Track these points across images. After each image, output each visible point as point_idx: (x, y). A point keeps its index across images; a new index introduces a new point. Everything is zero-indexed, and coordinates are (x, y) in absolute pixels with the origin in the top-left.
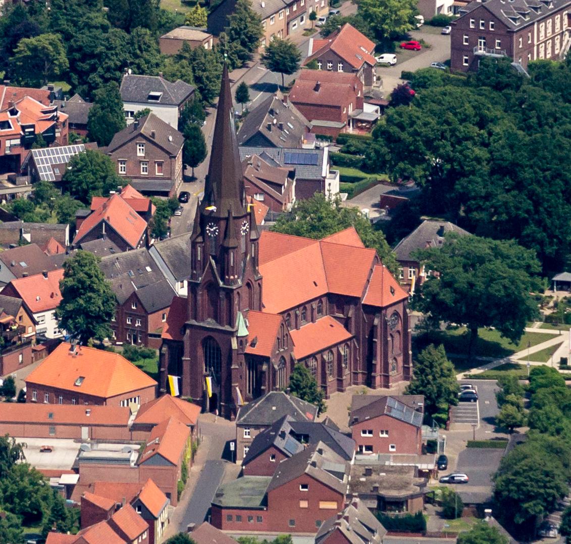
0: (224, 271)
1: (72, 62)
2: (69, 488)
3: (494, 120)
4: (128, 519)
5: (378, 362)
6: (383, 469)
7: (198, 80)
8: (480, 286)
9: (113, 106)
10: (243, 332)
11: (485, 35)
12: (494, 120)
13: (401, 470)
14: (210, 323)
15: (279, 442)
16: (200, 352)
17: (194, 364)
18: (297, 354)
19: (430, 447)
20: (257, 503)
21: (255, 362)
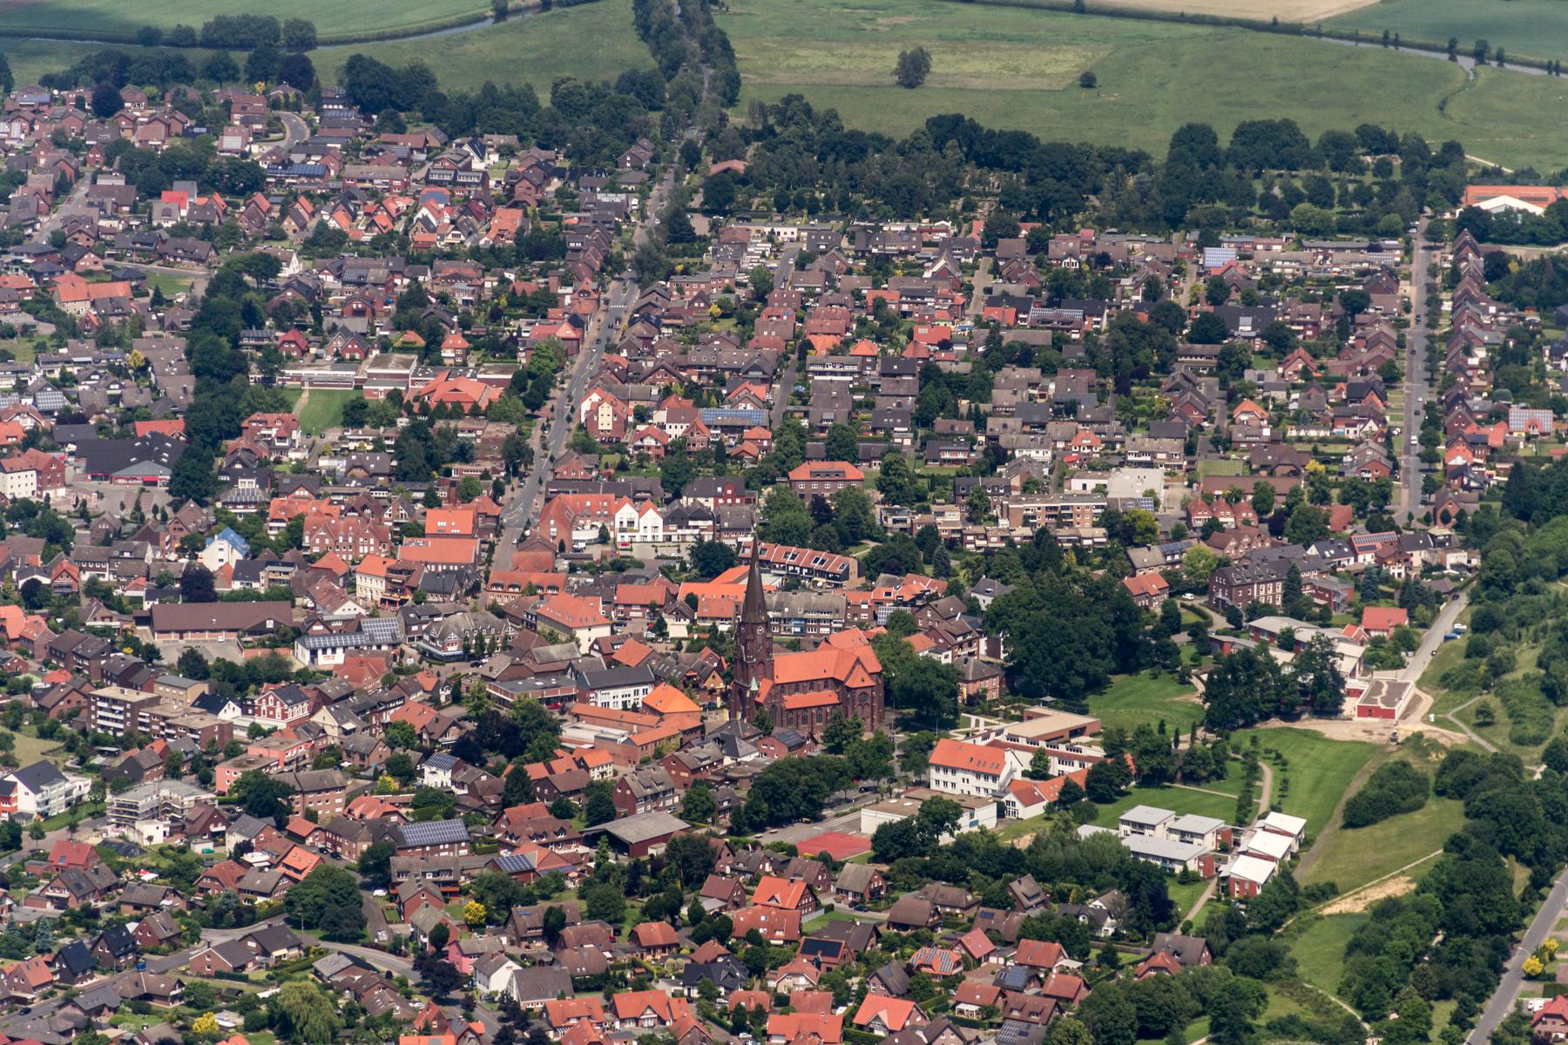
11: (1221, 586)
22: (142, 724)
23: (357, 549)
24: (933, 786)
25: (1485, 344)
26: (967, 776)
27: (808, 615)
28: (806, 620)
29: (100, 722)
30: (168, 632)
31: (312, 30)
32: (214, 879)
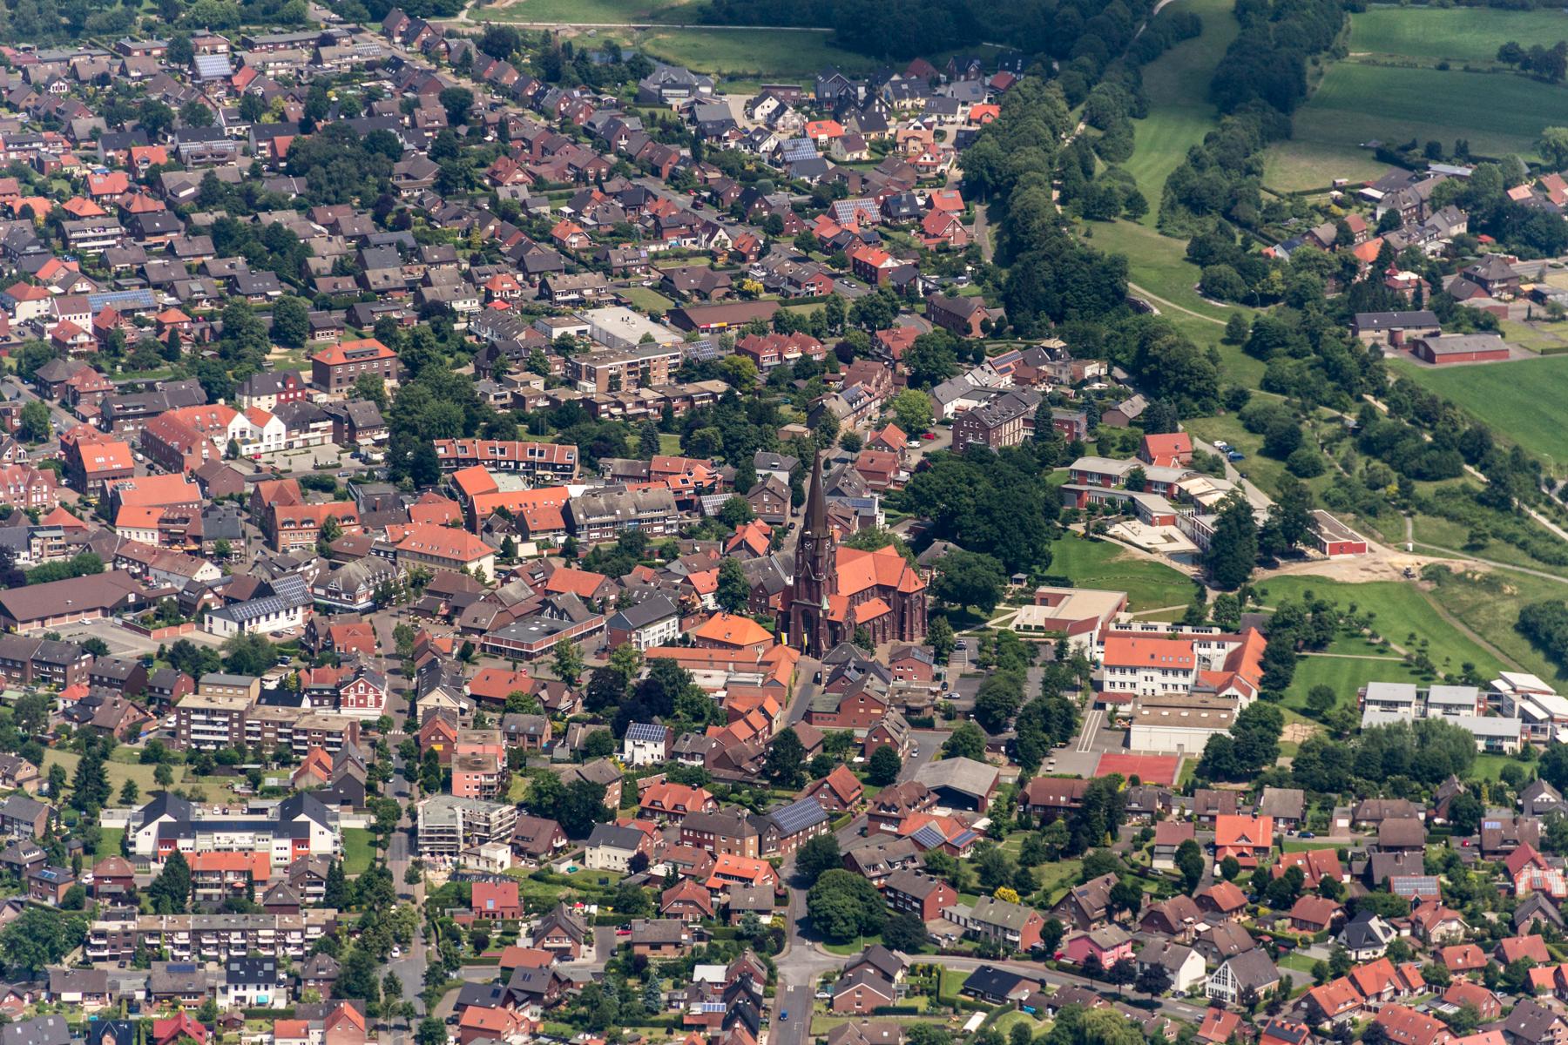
0: (815, 570)
1: (726, 444)
2: (721, 699)
5: (907, 626)
7: (801, 455)
8: (969, 581)
9: (749, 470)
10: (826, 607)
11: (973, 430)
13: (920, 691)
14: (806, 601)
18: (859, 621)
19: (938, 677)
20: (833, 709)
21: (833, 625)
22: (249, 733)
23: (28, 499)
24: (1107, 688)
26: (1149, 674)
27: (642, 515)
28: (640, 521)
29: (194, 736)
30: (30, 621)
31: (1517, 47)
32: (685, 902)
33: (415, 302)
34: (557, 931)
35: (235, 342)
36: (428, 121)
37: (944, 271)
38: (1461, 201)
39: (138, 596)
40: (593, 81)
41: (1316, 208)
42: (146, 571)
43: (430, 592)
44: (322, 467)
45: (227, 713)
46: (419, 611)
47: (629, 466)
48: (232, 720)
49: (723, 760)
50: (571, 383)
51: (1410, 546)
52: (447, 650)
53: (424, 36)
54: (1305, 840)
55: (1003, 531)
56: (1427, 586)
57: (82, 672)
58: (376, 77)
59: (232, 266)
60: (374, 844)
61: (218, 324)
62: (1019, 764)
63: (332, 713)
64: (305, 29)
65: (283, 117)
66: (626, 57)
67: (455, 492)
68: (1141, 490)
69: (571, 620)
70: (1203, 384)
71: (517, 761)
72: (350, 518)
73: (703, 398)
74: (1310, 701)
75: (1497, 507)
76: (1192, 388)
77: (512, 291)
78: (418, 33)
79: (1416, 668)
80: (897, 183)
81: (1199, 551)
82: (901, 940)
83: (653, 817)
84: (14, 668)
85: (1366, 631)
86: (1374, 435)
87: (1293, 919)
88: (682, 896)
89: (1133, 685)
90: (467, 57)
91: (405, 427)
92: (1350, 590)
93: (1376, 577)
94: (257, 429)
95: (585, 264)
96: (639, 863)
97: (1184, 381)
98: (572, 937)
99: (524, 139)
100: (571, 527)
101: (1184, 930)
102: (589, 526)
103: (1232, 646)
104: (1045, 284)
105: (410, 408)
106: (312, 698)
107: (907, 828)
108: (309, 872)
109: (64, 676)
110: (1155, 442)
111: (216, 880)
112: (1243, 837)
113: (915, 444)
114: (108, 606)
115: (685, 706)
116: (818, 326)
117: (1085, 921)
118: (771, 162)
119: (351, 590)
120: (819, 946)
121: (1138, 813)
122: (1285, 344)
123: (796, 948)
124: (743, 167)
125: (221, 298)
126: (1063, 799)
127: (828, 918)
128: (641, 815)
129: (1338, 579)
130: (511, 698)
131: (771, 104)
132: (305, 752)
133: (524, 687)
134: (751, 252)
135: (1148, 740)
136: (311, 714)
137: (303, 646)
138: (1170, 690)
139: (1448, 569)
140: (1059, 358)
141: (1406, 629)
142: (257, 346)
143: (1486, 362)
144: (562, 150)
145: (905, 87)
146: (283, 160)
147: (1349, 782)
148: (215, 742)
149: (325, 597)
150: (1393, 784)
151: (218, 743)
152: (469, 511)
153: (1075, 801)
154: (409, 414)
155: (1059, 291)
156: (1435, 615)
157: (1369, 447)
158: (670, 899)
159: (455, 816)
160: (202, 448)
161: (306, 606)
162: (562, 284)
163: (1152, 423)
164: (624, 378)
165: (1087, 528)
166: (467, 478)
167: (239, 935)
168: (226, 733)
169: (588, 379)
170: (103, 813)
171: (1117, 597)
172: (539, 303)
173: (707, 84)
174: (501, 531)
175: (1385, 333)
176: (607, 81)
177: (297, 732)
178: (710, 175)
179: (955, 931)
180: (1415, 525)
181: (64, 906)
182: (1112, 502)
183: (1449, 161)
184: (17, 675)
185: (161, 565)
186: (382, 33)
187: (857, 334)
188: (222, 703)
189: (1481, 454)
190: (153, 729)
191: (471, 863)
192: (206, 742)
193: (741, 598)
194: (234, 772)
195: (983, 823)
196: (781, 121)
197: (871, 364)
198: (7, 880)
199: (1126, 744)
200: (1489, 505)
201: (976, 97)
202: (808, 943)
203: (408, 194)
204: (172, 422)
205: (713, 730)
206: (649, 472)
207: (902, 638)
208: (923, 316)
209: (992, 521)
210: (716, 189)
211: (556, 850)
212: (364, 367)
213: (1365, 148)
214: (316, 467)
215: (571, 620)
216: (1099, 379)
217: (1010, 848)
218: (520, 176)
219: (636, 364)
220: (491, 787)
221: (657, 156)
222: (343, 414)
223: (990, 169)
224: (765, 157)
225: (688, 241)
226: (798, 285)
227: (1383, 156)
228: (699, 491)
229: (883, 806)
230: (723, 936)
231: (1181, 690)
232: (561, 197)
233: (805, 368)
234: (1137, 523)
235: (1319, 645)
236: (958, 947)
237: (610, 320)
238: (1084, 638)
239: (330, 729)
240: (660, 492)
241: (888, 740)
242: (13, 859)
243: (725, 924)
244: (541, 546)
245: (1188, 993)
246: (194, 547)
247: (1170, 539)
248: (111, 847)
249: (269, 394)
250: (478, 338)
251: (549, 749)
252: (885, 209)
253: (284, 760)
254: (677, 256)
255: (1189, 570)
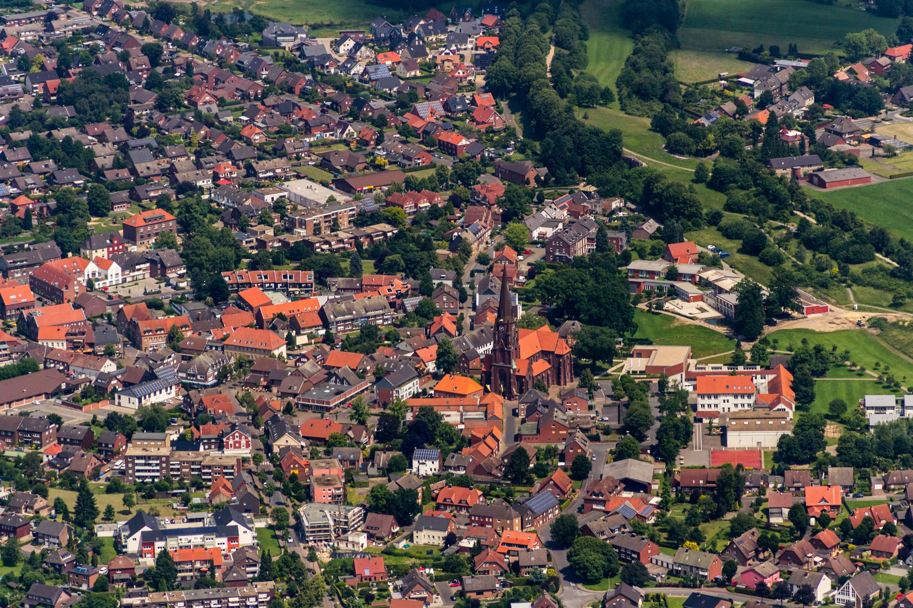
0: (507, 344)
1: (407, 265)
2: (461, 430)
3: (587, 281)
4: (489, 440)
5: (562, 376)
6: (578, 417)
7: (456, 270)
8: (599, 345)
9: (427, 280)
10: (514, 367)
11: (559, 247)
12: (587, 281)
13: (585, 417)
14: (501, 364)
15: (539, 409)
16: (498, 375)
17: (495, 380)
18: (534, 375)
19: (591, 408)
20: (535, 432)
21: (519, 378)
24: (700, 409)
25: (881, 147)
26: (726, 398)
27: (369, 314)
28: (368, 317)
29: (137, 474)
32: (490, 563)
33: (171, 184)
34: (418, 587)
35: (67, 215)
36: (138, 65)
37: (496, 145)
38: (808, 83)
39: (67, 385)
40: (231, 34)
41: (713, 92)
42: (68, 368)
43: (253, 371)
44: (151, 293)
45: (158, 458)
46: (247, 384)
47: (348, 282)
48: (162, 462)
49: (479, 469)
50: (289, 230)
51: (856, 306)
52: (278, 409)
53: (113, 11)
54: (858, 499)
55: (607, 311)
56: (874, 331)
57: (50, 436)
58: (93, 39)
59: (46, 166)
60: (275, 537)
61: (52, 203)
62: (663, 461)
63: (218, 453)
64: (33, 10)
65: (43, 67)
66: (248, 17)
67: (242, 305)
68: (675, 280)
69: (349, 384)
70: (693, 209)
71: (350, 479)
72: (186, 326)
73: (377, 236)
74: (831, 409)
75: (904, 278)
76: (686, 212)
77: (231, 173)
78: (109, 9)
79: (886, 384)
80: (449, 90)
81: (723, 317)
82: (634, 579)
83: (445, 509)
84: (6, 436)
85: (848, 363)
86: (812, 236)
87: (872, 551)
88: (488, 559)
89: (716, 406)
90: (146, 23)
91: (196, 265)
92: (817, 336)
93: (840, 328)
94: (102, 271)
95: (268, 153)
96: (451, 540)
97: (681, 208)
98: (427, 590)
99: (202, 74)
100: (326, 324)
101: (808, 562)
102: (337, 322)
103: (770, 377)
104: (570, 151)
105: (198, 252)
106: (204, 444)
107: (610, 507)
108: (248, 558)
109: (40, 439)
110: (674, 248)
111: (189, 567)
112: (823, 499)
113: (521, 257)
114: (49, 392)
115: (441, 436)
116: (434, 185)
117: (744, 561)
118: (360, 80)
119: (203, 372)
120: (580, 586)
121: (750, 488)
122: (735, 181)
123: (566, 588)
124: (345, 84)
125: (45, 187)
126: (701, 482)
127: (585, 568)
128: (437, 508)
129: (817, 330)
130: (332, 437)
131: (350, 44)
132: (210, 480)
133: (336, 430)
134: (371, 139)
135: (737, 440)
136: (209, 455)
137: (182, 411)
138: (740, 407)
139: (885, 320)
140: (593, 198)
141: (871, 360)
142: (82, 217)
143: (858, 185)
144: (229, 80)
145: (430, 27)
146: (53, 95)
147: (875, 460)
148: (151, 477)
149: (186, 379)
150: (902, 460)
151: (153, 477)
152: (258, 316)
153: (709, 482)
154: (198, 256)
155: (579, 154)
156: (885, 350)
157: (812, 243)
158: (481, 561)
159: (326, 516)
160: (74, 286)
161: (177, 385)
162: (264, 168)
163: (669, 236)
164: (323, 225)
165: (650, 306)
166: (250, 295)
167: (216, 602)
168: (158, 471)
169: (301, 227)
170: (96, 527)
171: (685, 350)
172: (249, 179)
173: (303, 32)
174: (283, 329)
175: (789, 170)
176: (239, 33)
177: (204, 467)
178: (327, 91)
179: (663, 572)
180: (854, 293)
181: (95, 589)
182: (660, 288)
183: (785, 58)
184: (9, 441)
185: (77, 363)
186: (83, 10)
187: (460, 188)
188: (153, 452)
189: (884, 245)
190: (107, 472)
191: (342, 546)
192: (146, 477)
193: (453, 364)
194: (168, 496)
195: (655, 500)
196: (358, 54)
197: (479, 208)
198: (52, 575)
199: (724, 442)
200: (899, 278)
201: (476, 32)
202: (573, 585)
203: (141, 114)
204: (49, 269)
205: (466, 450)
206: (362, 285)
207: (559, 384)
208: (493, 174)
209: (600, 305)
210: (335, 99)
211: (393, 533)
212: (156, 227)
213: (729, 52)
214: (145, 293)
215: (349, 384)
216: (620, 209)
217: (677, 514)
218: (208, 98)
219: (329, 216)
220: (339, 496)
221: (290, 80)
222: (157, 258)
223: (509, 78)
224: (357, 77)
225: (328, 134)
226: (409, 159)
227: (744, 57)
228: (400, 296)
229: (594, 493)
230: (519, 583)
231: (746, 408)
232: (236, 110)
233: (434, 212)
234: (678, 301)
235: (821, 373)
236: (669, 581)
237: (298, 188)
238: (677, 377)
239: (225, 464)
240: (378, 299)
241: (579, 451)
242: (55, 561)
243: (517, 576)
244: (311, 337)
245: (823, 602)
246: (90, 350)
247: (702, 310)
248: (109, 549)
249: (103, 248)
250: (218, 204)
251: (364, 469)
252: (446, 106)
253: (199, 487)
254: (323, 145)
255: (722, 330)
